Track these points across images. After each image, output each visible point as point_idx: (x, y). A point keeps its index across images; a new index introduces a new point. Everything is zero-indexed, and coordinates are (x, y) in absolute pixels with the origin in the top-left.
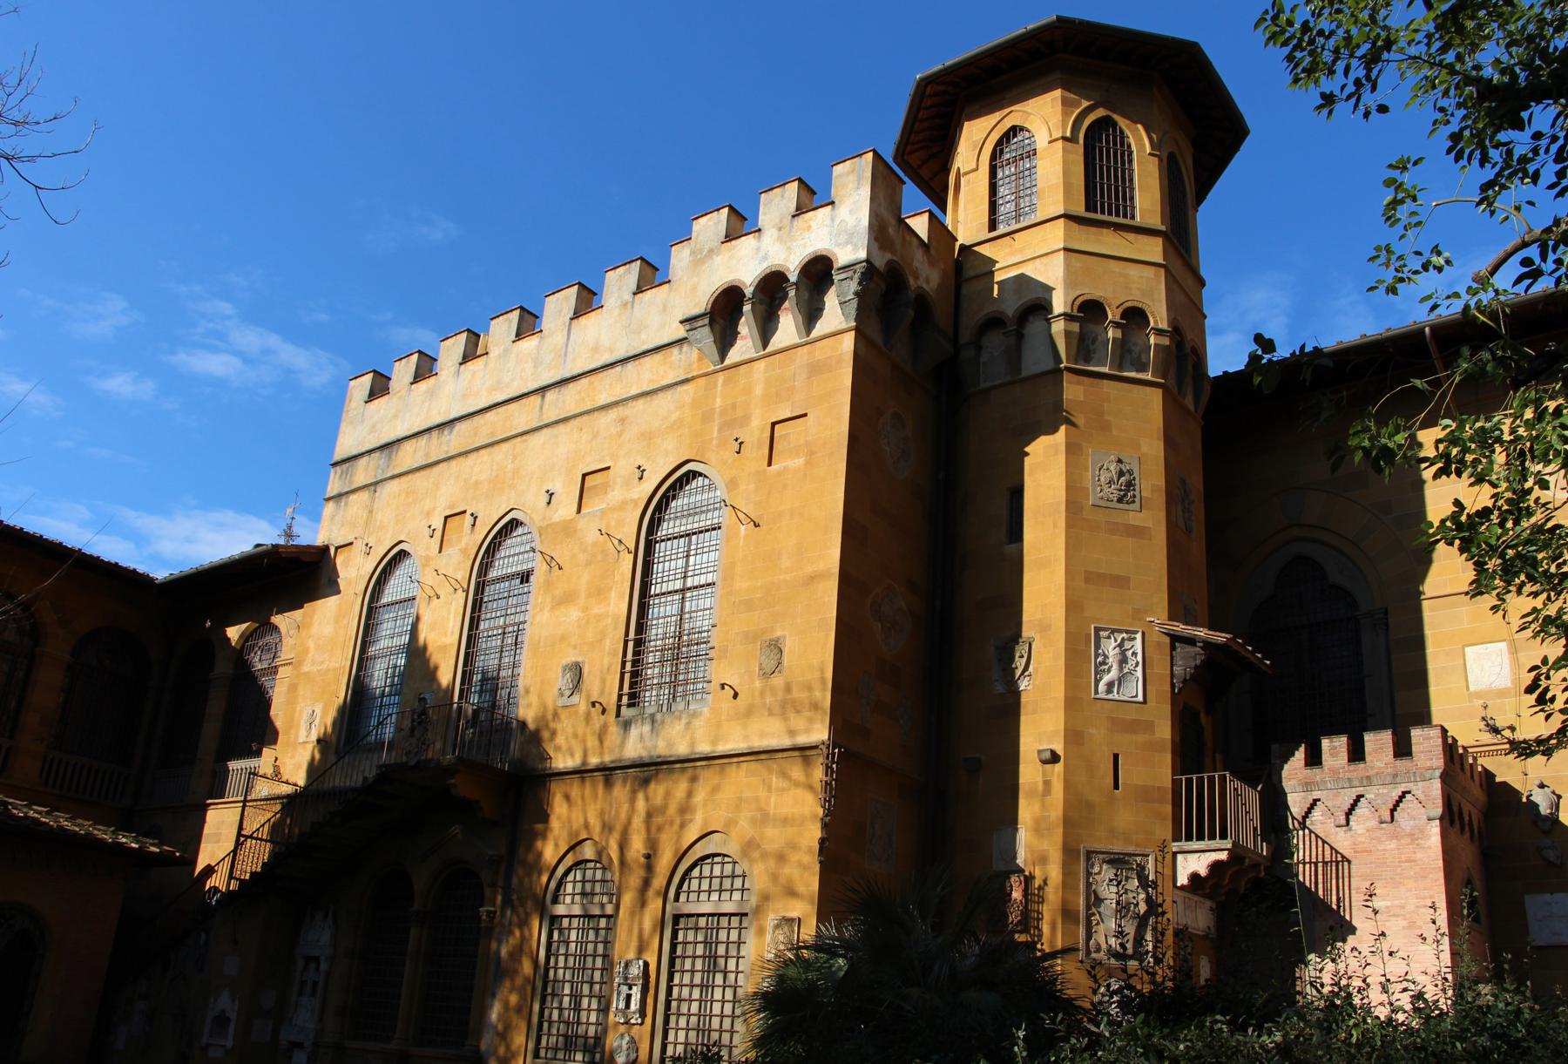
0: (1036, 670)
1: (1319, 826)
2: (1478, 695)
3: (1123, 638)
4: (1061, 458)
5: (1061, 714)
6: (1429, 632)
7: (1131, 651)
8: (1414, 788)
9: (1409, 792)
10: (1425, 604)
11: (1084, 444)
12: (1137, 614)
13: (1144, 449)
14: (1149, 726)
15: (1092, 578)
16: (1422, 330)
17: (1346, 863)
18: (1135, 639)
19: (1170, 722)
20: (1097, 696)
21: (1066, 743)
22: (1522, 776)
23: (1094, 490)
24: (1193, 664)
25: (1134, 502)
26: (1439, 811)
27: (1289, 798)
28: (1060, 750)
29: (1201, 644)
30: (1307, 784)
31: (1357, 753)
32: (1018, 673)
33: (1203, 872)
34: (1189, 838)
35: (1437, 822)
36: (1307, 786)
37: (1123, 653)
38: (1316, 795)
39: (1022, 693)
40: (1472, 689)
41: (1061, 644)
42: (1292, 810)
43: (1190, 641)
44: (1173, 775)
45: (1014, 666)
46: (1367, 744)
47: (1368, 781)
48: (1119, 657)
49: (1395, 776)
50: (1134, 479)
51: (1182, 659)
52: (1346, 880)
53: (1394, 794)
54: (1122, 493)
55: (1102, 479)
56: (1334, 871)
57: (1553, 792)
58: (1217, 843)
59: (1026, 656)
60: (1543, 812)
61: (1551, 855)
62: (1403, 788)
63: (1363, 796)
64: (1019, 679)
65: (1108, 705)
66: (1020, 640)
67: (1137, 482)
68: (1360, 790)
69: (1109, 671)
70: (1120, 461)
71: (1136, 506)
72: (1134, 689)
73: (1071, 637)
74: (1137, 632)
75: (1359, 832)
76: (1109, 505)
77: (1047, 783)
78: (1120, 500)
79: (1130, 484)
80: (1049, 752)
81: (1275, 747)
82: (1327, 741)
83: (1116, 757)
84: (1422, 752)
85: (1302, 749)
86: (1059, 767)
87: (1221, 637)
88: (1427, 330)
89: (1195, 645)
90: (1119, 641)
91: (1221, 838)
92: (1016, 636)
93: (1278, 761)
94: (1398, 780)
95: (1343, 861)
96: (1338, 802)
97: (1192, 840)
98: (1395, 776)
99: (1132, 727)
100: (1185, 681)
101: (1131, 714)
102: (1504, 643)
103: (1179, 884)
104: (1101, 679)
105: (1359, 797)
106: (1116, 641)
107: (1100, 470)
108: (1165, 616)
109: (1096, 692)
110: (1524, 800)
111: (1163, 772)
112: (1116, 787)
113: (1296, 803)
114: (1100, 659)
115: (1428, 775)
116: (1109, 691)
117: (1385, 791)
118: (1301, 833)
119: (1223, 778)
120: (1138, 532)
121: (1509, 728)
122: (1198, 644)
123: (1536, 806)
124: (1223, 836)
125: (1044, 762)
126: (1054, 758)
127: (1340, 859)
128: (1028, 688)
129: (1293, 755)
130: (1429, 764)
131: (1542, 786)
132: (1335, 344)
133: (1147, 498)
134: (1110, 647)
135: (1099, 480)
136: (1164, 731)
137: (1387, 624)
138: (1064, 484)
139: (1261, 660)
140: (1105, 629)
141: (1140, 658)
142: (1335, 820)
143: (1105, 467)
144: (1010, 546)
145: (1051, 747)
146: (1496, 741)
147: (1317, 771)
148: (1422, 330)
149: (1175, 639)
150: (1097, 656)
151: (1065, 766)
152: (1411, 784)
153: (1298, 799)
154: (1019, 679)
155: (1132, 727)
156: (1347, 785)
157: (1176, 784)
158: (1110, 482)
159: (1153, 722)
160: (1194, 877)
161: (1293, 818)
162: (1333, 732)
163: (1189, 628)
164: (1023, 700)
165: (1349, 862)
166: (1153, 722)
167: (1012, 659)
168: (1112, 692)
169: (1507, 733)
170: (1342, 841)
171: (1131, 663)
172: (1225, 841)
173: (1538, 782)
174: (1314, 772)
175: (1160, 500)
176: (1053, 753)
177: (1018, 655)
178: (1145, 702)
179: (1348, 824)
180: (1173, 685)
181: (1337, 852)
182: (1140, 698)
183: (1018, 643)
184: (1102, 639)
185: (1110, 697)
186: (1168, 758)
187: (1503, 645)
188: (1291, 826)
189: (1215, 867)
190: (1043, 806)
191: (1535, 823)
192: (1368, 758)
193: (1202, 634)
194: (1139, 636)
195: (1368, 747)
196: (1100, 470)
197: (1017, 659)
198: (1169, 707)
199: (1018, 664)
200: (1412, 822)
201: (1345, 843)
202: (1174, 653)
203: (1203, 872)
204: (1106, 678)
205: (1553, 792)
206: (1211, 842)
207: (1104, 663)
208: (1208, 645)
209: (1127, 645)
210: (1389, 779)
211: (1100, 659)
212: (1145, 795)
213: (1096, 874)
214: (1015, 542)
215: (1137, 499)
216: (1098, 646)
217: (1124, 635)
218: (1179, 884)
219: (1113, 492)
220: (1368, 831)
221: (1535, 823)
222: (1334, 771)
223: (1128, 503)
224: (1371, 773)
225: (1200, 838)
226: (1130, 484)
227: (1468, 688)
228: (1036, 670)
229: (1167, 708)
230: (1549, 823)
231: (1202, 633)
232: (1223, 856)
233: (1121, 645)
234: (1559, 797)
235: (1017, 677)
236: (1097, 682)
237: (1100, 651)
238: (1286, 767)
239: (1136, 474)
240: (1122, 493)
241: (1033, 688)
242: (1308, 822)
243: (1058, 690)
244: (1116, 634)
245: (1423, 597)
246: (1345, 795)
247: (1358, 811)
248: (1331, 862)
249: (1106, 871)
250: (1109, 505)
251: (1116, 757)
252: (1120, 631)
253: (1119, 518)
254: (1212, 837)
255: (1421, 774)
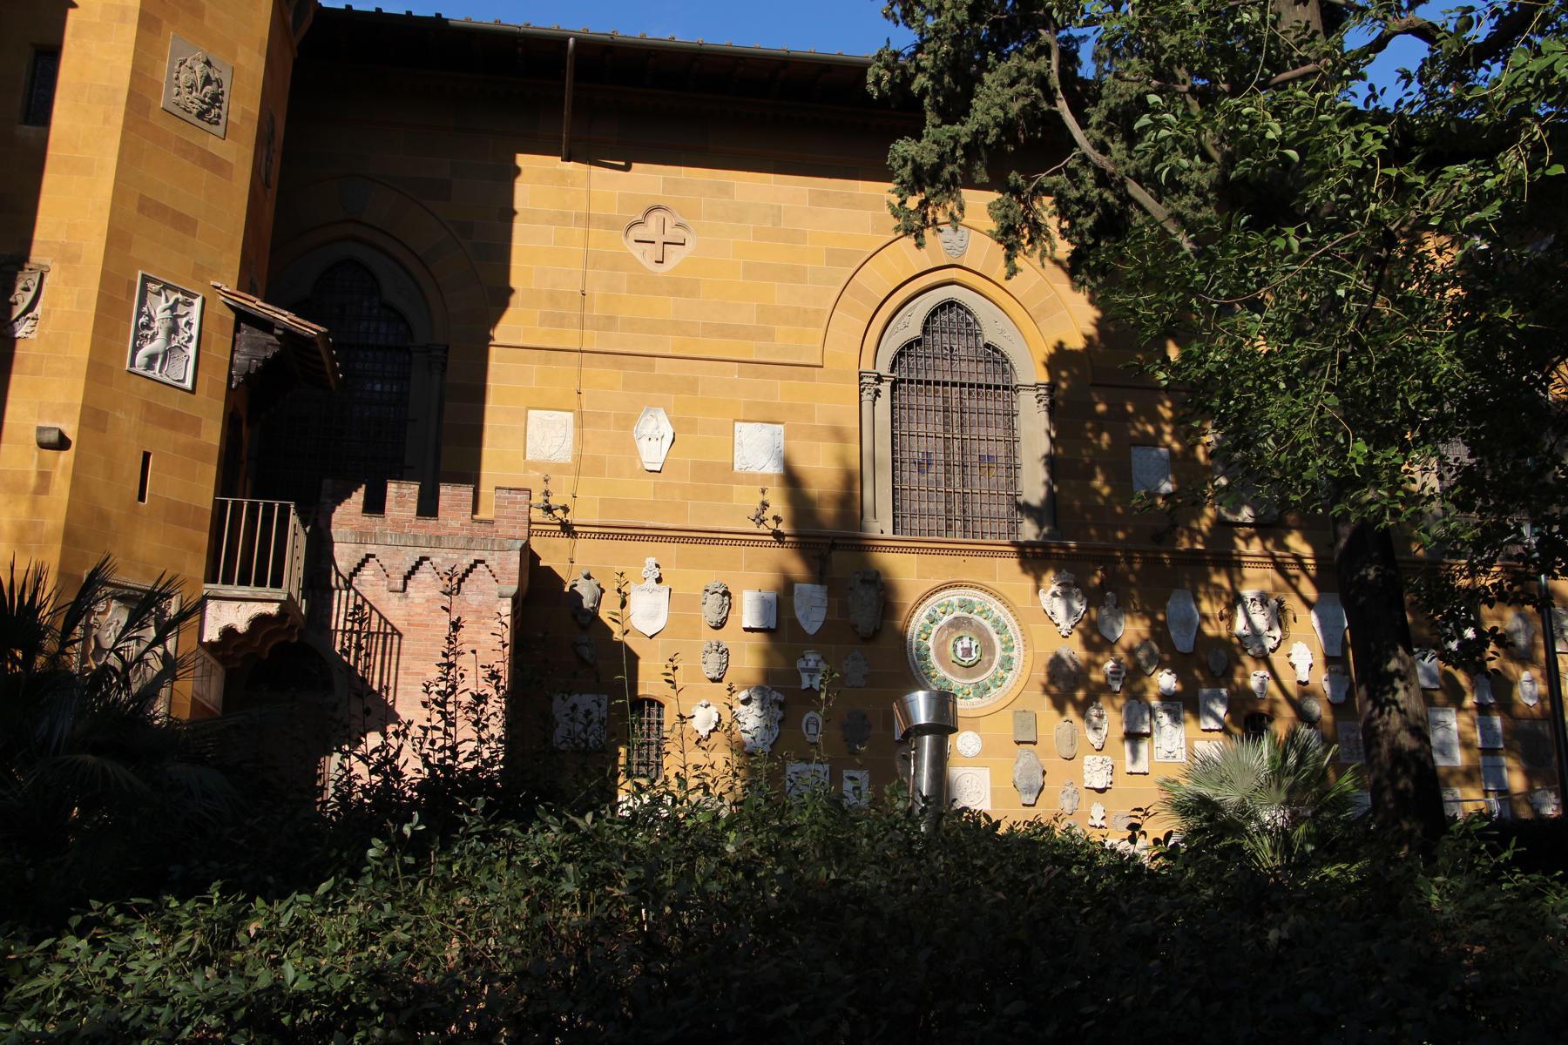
0: (47, 313)
1: (369, 588)
2: (535, 466)
3: (177, 301)
4: (131, 30)
5: (80, 384)
6: (492, 383)
7: (184, 320)
8: (490, 557)
9: (482, 562)
10: (493, 351)
11: (165, 22)
12: (200, 272)
13: (241, 60)
14: (194, 425)
15: (148, 207)
16: (565, 40)
17: (396, 637)
18: (191, 304)
19: (220, 425)
20: (133, 369)
21: (82, 423)
22: (569, 564)
23: (169, 89)
24: (262, 355)
25: (217, 123)
26: (513, 589)
27: (336, 549)
28: (71, 432)
29: (280, 332)
30: (362, 534)
31: (428, 507)
32: (17, 311)
33: (242, 627)
34: (228, 580)
35: (509, 601)
36: (362, 537)
37: (175, 318)
38: (371, 549)
39: (18, 341)
40: (529, 457)
41: (94, 287)
42: (338, 563)
43: (266, 325)
44: (215, 495)
45: (12, 300)
46: (441, 497)
47: (437, 541)
48: (169, 323)
49: (471, 540)
50: (222, 93)
51: (247, 345)
52: (394, 657)
53: (465, 562)
54: (205, 107)
55: (182, 78)
56: (380, 645)
57: (599, 586)
58: (267, 591)
59: (33, 290)
60: (585, 606)
61: (586, 653)
62: (476, 555)
63: (427, 559)
64: (17, 320)
65: (145, 384)
66: (27, 266)
67: (225, 98)
68: (426, 551)
69: (153, 339)
70: (208, 63)
71: (219, 130)
72: (182, 371)
73: (107, 280)
74: (195, 296)
75: (417, 601)
76: (186, 116)
77: (44, 477)
78: (201, 115)
79: (216, 99)
80: (57, 432)
81: (327, 483)
82: (394, 485)
83: (146, 456)
84: (506, 517)
85: (362, 490)
86: (66, 457)
87: (311, 329)
88: (571, 41)
89: (271, 333)
90: (171, 301)
91: (272, 586)
92: (20, 258)
93: (329, 501)
94: (473, 545)
95: (392, 634)
96: (397, 562)
97: (231, 583)
98: (471, 540)
99: (174, 421)
100: (247, 376)
101: (174, 403)
102: (571, 414)
103: (205, 640)
104: (141, 347)
105: (423, 559)
106: (167, 300)
107: (181, 64)
108: (234, 283)
109: (133, 364)
110: (567, 589)
111: (202, 489)
112: (142, 497)
113: (344, 555)
114: (143, 320)
115: (507, 545)
116: (149, 366)
117: (456, 556)
118: (344, 593)
119: (284, 512)
120: (216, 165)
121: (562, 508)
122: (277, 331)
123: (579, 597)
124: (277, 583)
125: (43, 445)
126: (62, 443)
127: (389, 630)
128: (30, 336)
129: (349, 496)
130: (511, 533)
131: (588, 577)
132: (492, 21)
133: (234, 124)
134: (159, 307)
135: (177, 78)
136: (212, 434)
137: (444, 365)
138: (129, 66)
139: (335, 371)
140: (156, 281)
141: (195, 331)
142: (389, 583)
143: (188, 63)
144: (26, 127)
145: (58, 426)
146: (547, 520)
147: (377, 520)
148: (565, 40)
149: (243, 317)
150: (140, 314)
151: (77, 456)
152: (486, 553)
153: (347, 551)
154: (17, 320)
155: (174, 421)
156: (411, 542)
157: (219, 508)
158: (191, 87)
159: (199, 420)
160: (228, 632)
161: (338, 574)
162: (401, 476)
163: (269, 307)
164: (20, 350)
165: (400, 636)
166: (199, 420)
167: (10, 289)
168: (153, 368)
169: (559, 513)
170: (394, 609)
171: (181, 338)
172: (278, 590)
173: (585, 573)
174: (374, 523)
175: (250, 132)
176: (62, 435)
177: (20, 285)
178: (193, 391)
179: (404, 590)
180: (230, 377)
181: (387, 622)
182: (188, 384)
183: (22, 269)
184: (149, 295)
185: (150, 373)
186: (212, 471)
187: (569, 417)
188: (334, 584)
189: (259, 622)
190: (34, 507)
191: (575, 616)
192: (441, 514)
193: (285, 319)
194: (198, 302)
195: (443, 502)
196: (181, 64)
197: (18, 290)
198: (222, 404)
199: (19, 298)
200: (480, 597)
201: (398, 612)
202: (238, 335)
203: (242, 627)
204: (148, 348)
205: (599, 586)
206: (258, 589)
207: (147, 326)
208: (290, 335)
209: (181, 310)
210: (462, 543)
211: (143, 320)
212: (178, 514)
213: (99, 613)
214: (35, 123)
215: (223, 122)
216: (142, 302)
217: (179, 295)
218: (205, 640)
219: (194, 101)
220: (428, 601)
221: (575, 616)
222: (398, 524)
223: (209, 122)
224: (443, 532)
225: (244, 581)
226: (216, 99)
227: (525, 457)
228: (47, 313)
229: (219, 406)
230: (589, 618)
231: (285, 317)
232: (273, 609)
233: (173, 308)
234: (603, 591)
235: (15, 316)
236: (135, 350)
237: (145, 309)
238: (338, 509)
239: (226, 88)
240: (205, 107)
241: (39, 338)
242: (355, 581)
243: (80, 349)
244: (168, 292)
245: (491, 343)
246: (407, 554)
247: (418, 576)
248: (378, 633)
249: (114, 611)
250: (186, 116)
251: (146, 456)
252: (175, 290)
253: (197, 139)
254: (261, 582)
255: (501, 543)
